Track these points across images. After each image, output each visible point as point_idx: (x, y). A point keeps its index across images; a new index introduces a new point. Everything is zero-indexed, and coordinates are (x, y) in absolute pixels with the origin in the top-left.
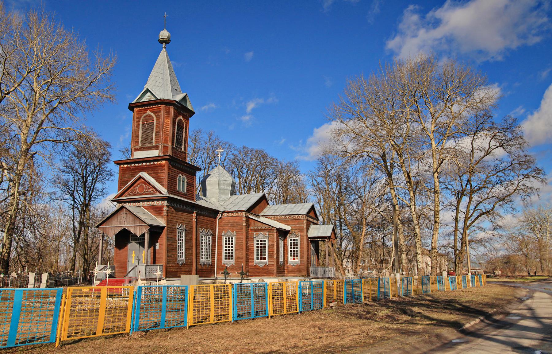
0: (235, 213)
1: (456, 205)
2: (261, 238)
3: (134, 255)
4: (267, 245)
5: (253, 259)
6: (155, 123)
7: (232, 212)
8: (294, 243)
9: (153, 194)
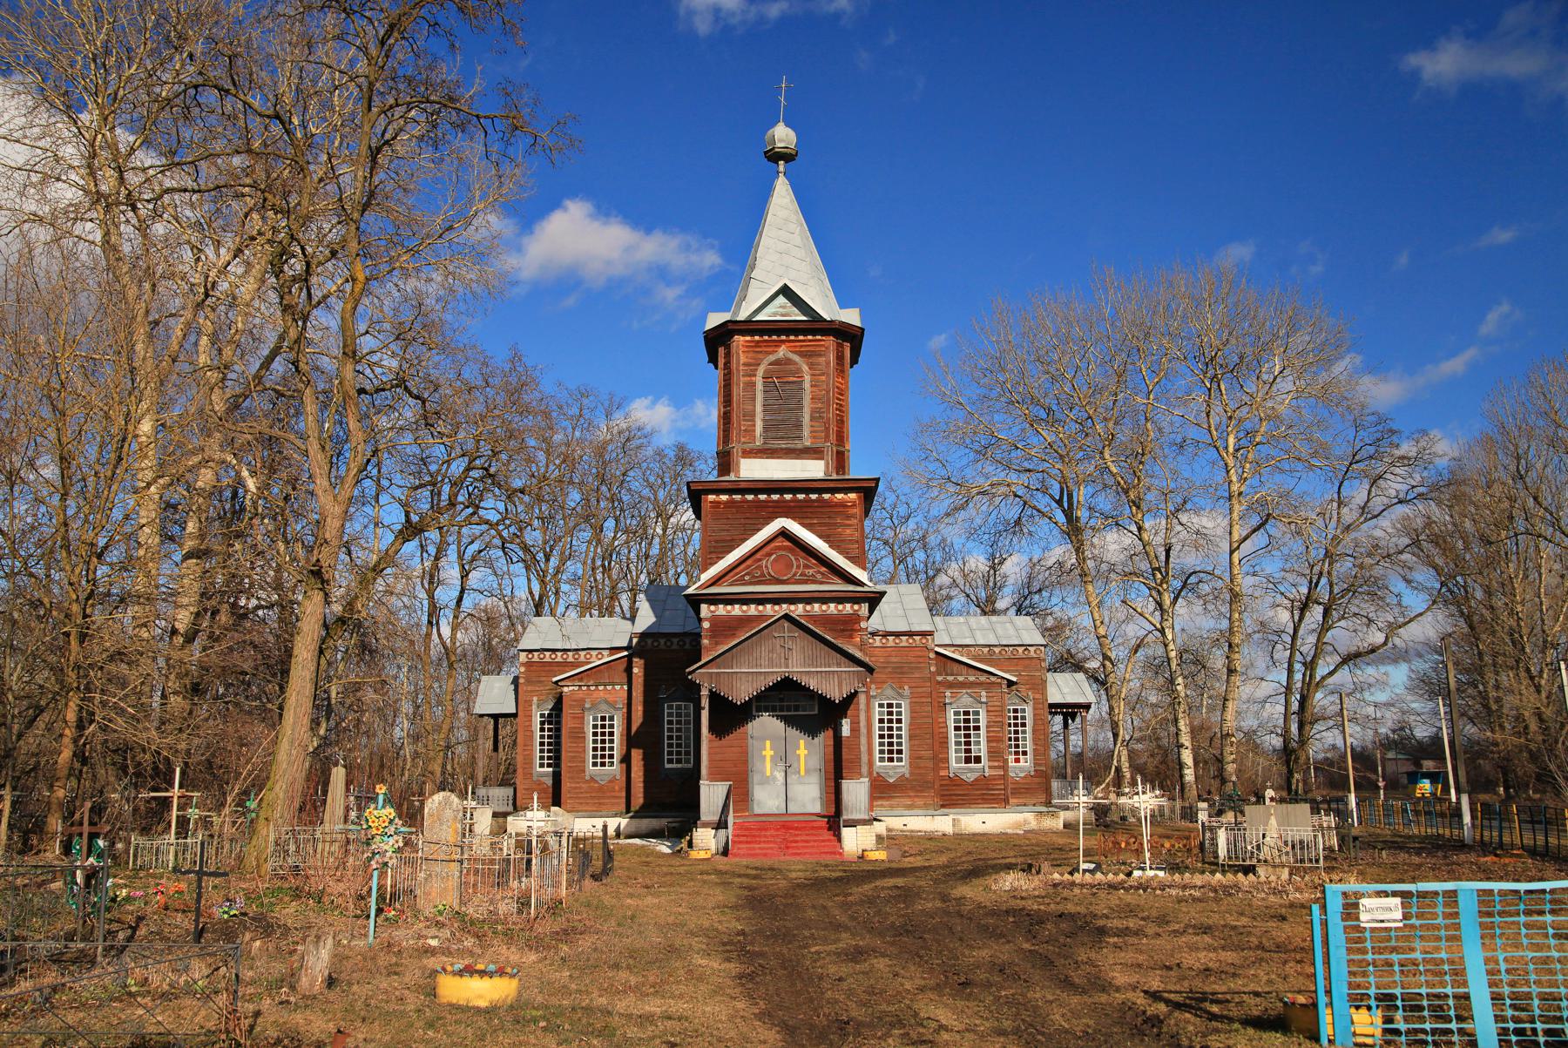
0: (904, 638)
1: (1291, 632)
2: (966, 706)
3: (768, 753)
4: (982, 724)
5: (947, 760)
6: (807, 385)
7: (897, 634)
8: (603, 726)
9: (821, 583)
